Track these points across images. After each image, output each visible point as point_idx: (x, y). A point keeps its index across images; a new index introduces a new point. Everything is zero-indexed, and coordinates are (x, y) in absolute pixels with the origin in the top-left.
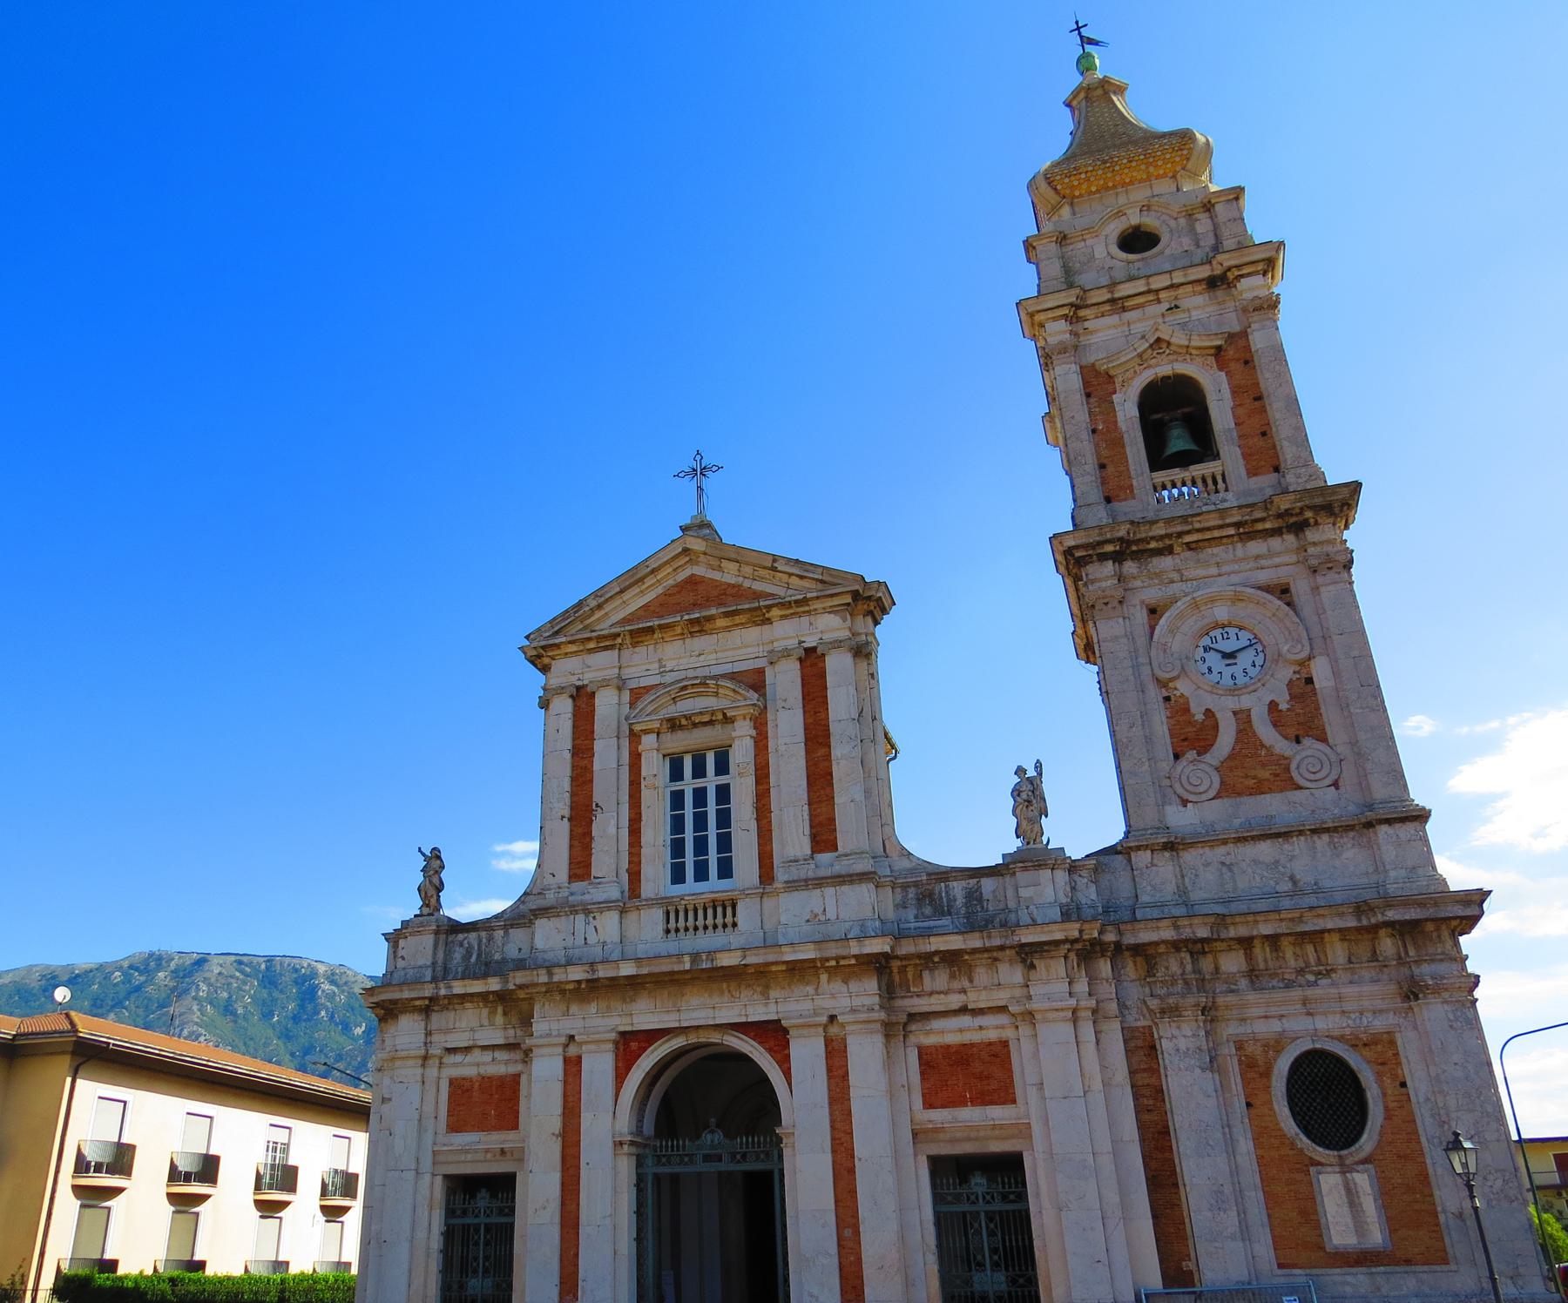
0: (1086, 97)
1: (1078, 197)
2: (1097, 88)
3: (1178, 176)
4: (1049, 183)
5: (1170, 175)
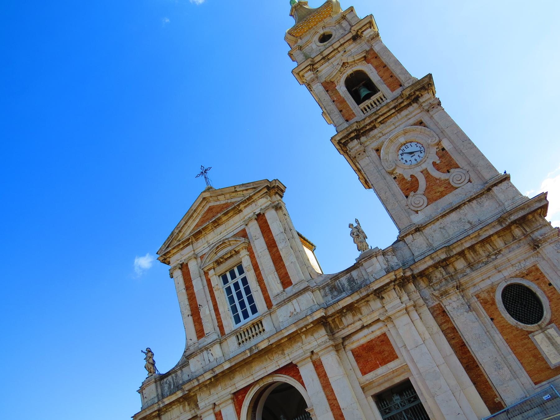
0: (296, 10)
1: (302, 35)
2: (298, 6)
3: (331, 15)
4: (290, 35)
5: (329, 15)
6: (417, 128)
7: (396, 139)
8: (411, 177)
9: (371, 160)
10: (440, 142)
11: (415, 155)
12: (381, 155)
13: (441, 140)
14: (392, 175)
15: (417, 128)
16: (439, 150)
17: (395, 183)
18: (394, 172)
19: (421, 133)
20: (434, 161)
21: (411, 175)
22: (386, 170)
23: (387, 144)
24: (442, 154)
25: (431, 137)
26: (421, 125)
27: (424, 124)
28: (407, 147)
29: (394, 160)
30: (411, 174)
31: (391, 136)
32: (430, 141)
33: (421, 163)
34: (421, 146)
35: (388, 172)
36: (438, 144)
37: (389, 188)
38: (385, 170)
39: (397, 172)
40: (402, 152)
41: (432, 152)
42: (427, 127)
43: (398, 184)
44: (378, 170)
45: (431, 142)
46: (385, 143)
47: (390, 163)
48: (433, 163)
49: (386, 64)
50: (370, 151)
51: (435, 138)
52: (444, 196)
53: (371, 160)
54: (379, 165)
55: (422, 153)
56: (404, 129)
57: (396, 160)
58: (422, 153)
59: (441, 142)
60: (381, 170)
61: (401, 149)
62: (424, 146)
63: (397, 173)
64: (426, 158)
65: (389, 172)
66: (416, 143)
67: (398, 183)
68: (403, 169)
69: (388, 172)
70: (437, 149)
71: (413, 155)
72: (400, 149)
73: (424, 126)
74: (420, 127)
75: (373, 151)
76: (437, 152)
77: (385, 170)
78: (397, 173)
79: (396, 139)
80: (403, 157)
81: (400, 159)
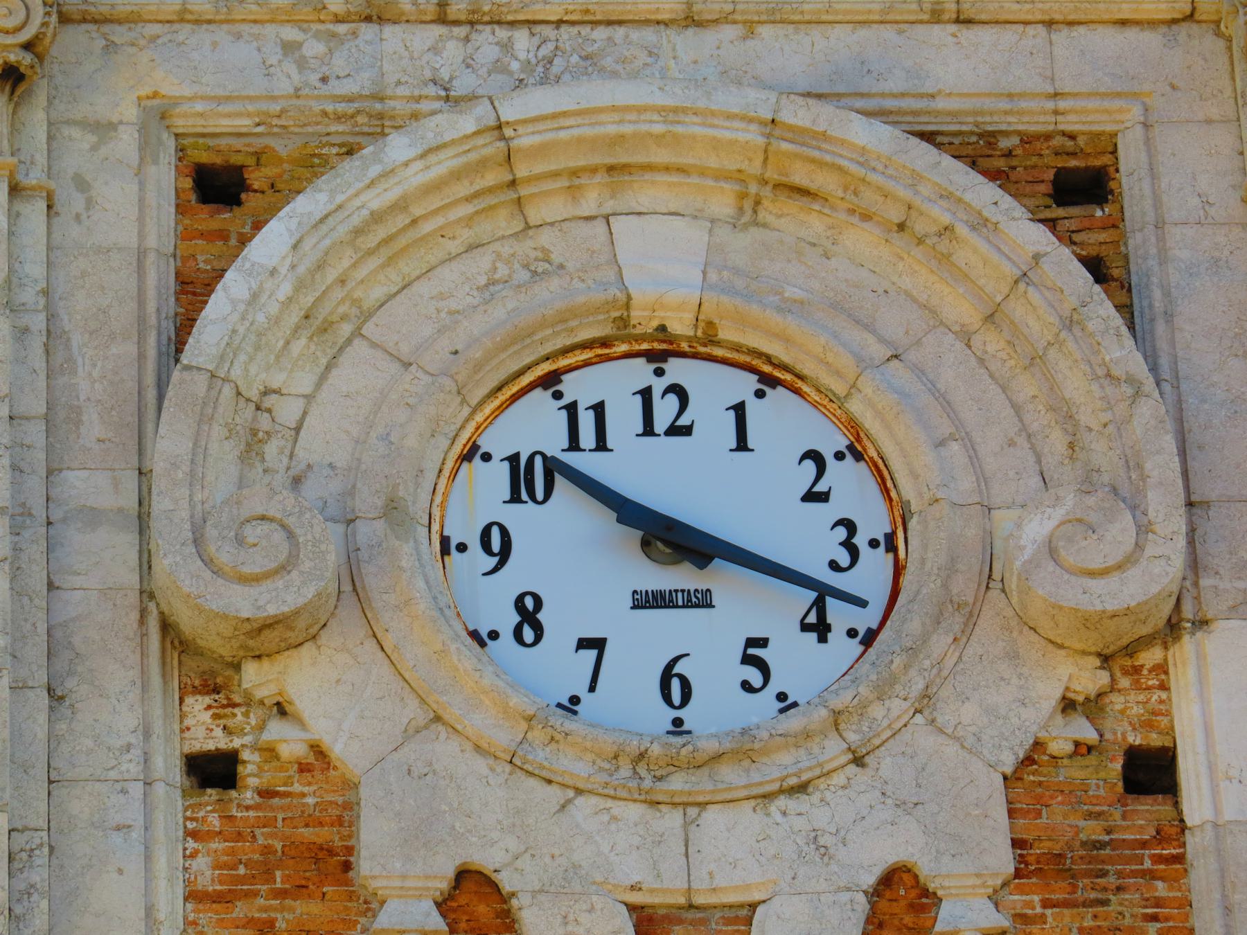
6: (981, 224)
7: (590, 203)
8: (443, 905)
9: (35, 269)
10: (1173, 629)
11: (702, 600)
12: (233, 285)
13: (1202, 623)
14: (198, 705)
15: (981, 224)
16: (1082, 749)
17: (166, 860)
18: (254, 677)
19: (992, 342)
20: (926, 868)
21: (464, 875)
22: (162, 564)
23: (416, 177)
24: (1093, 830)
25: (1087, 485)
26: (1073, 214)
27: (1114, 224)
28: (665, 410)
29: (368, 501)
30: (486, 859)
31: (540, 101)
32: (1036, 528)
33: (732, 775)
34: (873, 523)
35: (166, 626)
36: (1130, 650)
37: (38, 876)
38: (146, 565)
39: (303, 703)
40: (555, 444)
41: (969, 712)
42: (1126, 310)
43: (193, 895)
44: (35, 486)
45: (1051, 550)
46: (398, 147)
47: (281, 503)
48: (891, 879)
49: (1194, 898)
50: (104, 129)
51: (1144, 529)
52: (92, 509)
53: (35, 269)
54: (93, 428)
55: (821, 629)
56: (797, 114)
57: (393, 510)
58: (821, 629)
59: (1188, 644)
60: (93, 517)
61: (572, 387)
62: (915, 549)
63: (281, 710)
64: (833, 750)
65: (186, 621)
66: (831, 441)
67: (205, 872)
68: (412, 711)
69: (166, 626)
70: (1068, 705)
71: (681, 578)
72: (550, 381)
73: (1097, 268)
74: (1037, 237)
75: (146, 147)
76: (1034, 755)
77: (146, 565)
78: (281, 710)
79: (590, 203)
80: (521, 519)
81: (465, 529)
